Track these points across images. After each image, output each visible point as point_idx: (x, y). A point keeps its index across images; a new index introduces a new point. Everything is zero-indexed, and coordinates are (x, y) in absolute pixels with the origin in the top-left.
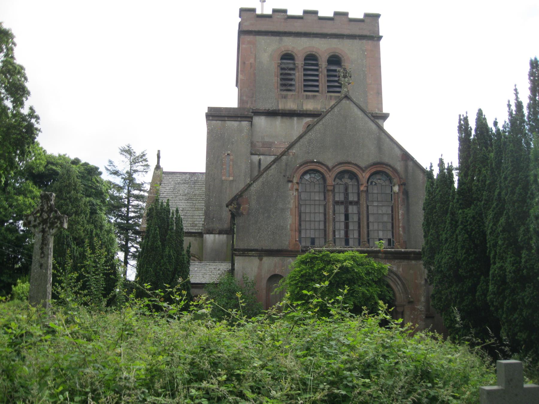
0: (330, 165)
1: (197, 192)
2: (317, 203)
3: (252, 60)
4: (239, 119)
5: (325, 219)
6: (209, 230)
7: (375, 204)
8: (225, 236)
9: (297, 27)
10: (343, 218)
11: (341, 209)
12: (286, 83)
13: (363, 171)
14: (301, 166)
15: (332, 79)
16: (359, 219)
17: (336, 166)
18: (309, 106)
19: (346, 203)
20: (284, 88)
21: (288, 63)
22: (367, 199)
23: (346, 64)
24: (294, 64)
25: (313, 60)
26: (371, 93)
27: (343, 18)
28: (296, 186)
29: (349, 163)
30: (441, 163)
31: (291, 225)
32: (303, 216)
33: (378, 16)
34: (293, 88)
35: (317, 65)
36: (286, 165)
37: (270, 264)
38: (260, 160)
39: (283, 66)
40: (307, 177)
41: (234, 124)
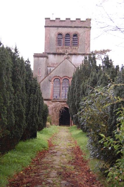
0: (61, 77)
3: (49, 36)
9: (63, 24)
12: (59, 42)
20: (59, 45)
21: (60, 37)
25: (68, 35)
28: (52, 83)
29: (64, 77)
33: (90, 20)
39: (58, 37)
40: (55, 80)
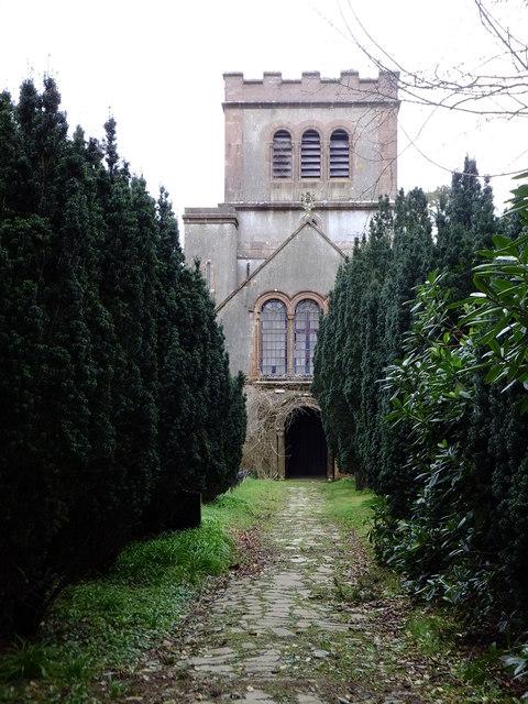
0: (291, 294)
3: (239, 142)
4: (220, 221)
12: (280, 167)
15: (337, 160)
24: (290, 143)
28: (257, 316)
31: (441, 222)
32: (264, 345)
35: (318, 143)
38: (248, 265)
40: (268, 306)
41: (215, 227)
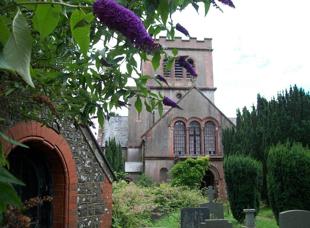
0: (187, 119)
1: (122, 127)
2: (182, 135)
5: (185, 143)
6: (130, 146)
7: (208, 136)
8: (138, 149)
10: (193, 142)
11: (192, 138)
13: (202, 121)
14: (174, 119)
16: (200, 143)
17: (189, 119)
18: (178, 85)
19: (194, 135)
22: (204, 134)
23: (196, 64)
26: (208, 77)
27: (194, 40)
30: (245, 109)
33: (211, 39)
34: (169, 75)
36: (168, 119)
37: (162, 164)
40: (177, 124)
